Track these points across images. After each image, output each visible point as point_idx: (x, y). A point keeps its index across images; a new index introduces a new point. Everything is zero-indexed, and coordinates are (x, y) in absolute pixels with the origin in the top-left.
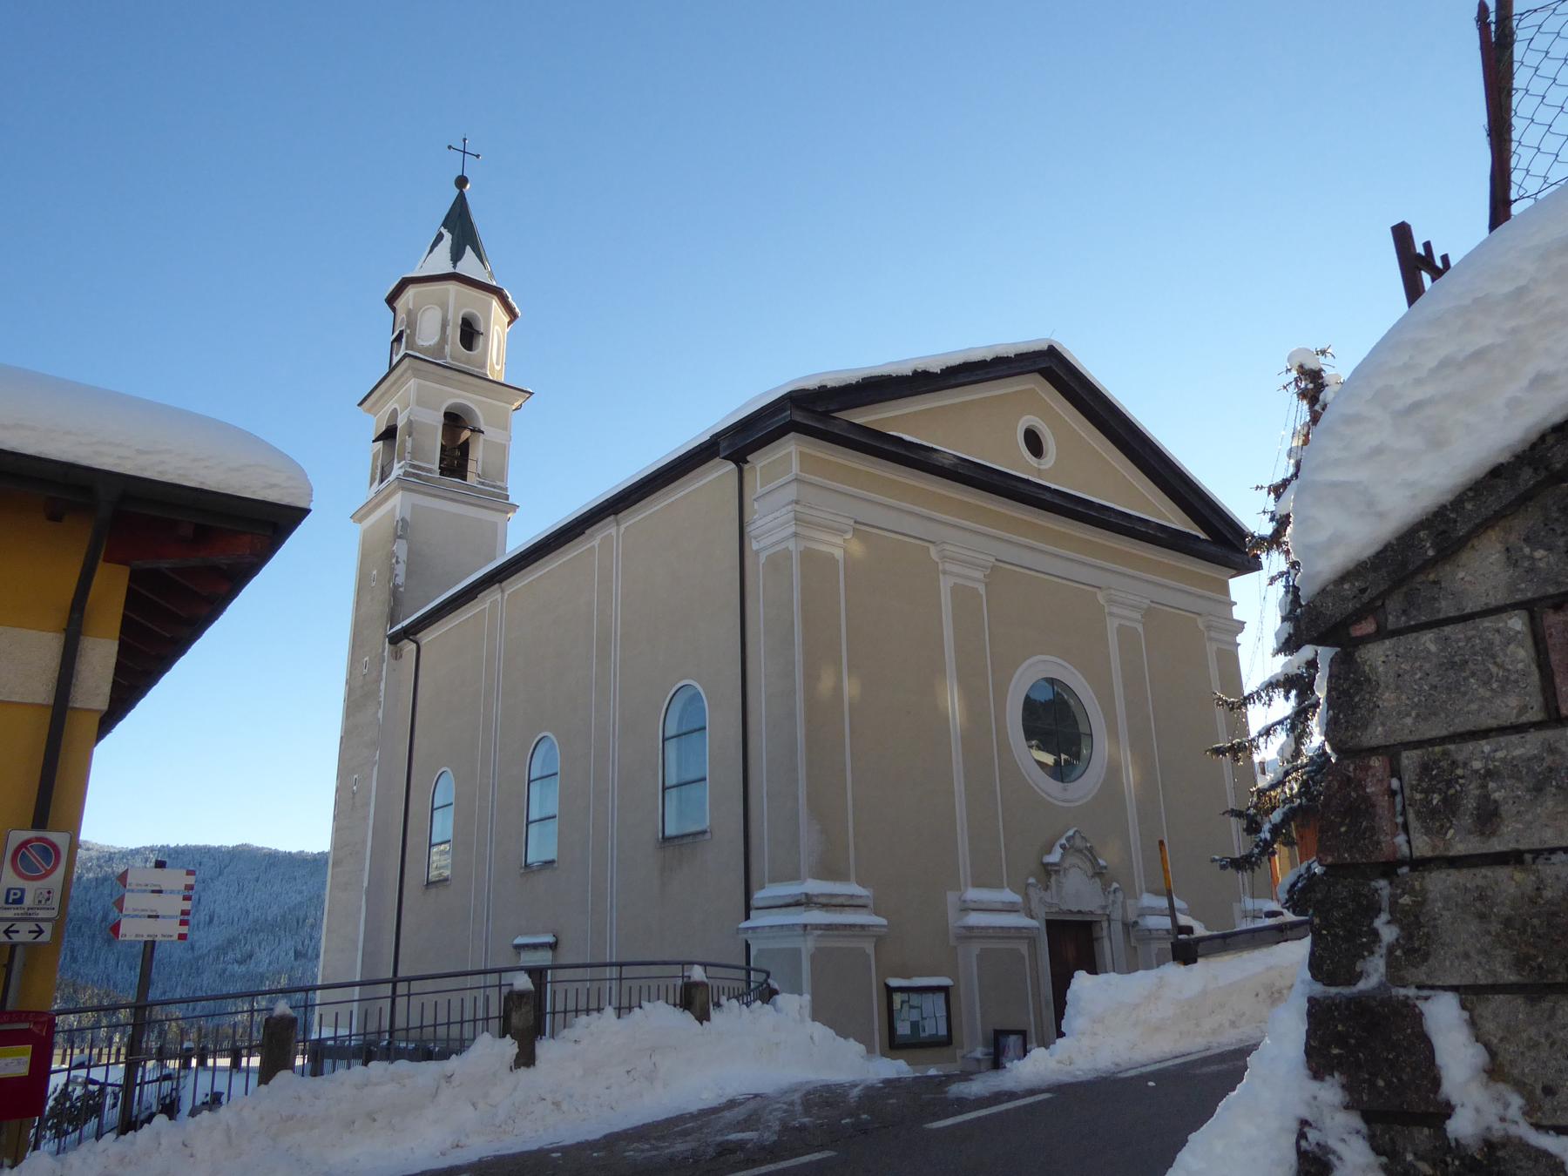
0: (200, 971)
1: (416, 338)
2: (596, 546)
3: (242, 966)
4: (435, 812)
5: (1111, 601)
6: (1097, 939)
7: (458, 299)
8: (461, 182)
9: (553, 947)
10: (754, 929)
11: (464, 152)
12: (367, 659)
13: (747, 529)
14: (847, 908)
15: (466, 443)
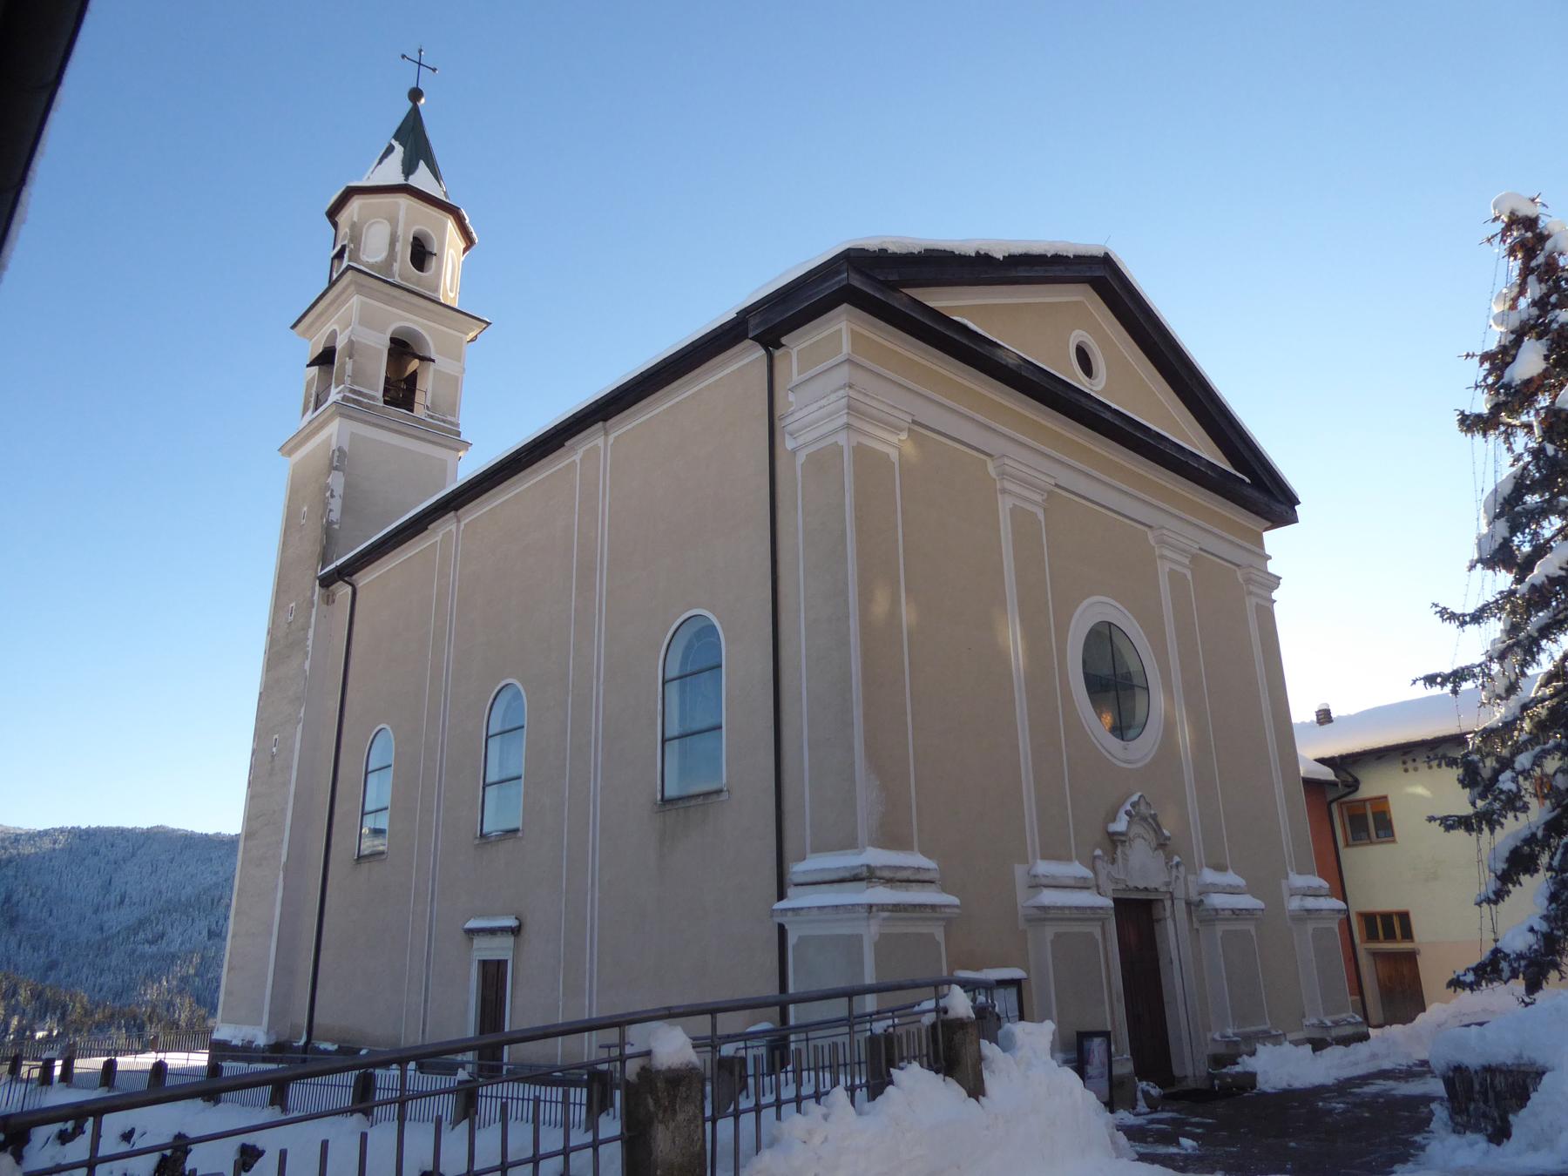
0: (109, 951)
1: (361, 254)
2: (578, 461)
3: (152, 946)
4: (370, 776)
5: (1162, 542)
6: (1159, 921)
7: (410, 216)
8: (416, 94)
9: (516, 931)
10: (795, 910)
11: (420, 64)
12: (293, 604)
13: (778, 425)
14: (914, 884)
15: (414, 374)
